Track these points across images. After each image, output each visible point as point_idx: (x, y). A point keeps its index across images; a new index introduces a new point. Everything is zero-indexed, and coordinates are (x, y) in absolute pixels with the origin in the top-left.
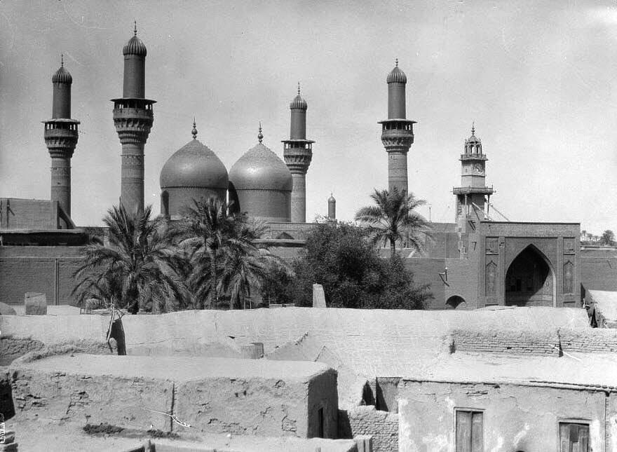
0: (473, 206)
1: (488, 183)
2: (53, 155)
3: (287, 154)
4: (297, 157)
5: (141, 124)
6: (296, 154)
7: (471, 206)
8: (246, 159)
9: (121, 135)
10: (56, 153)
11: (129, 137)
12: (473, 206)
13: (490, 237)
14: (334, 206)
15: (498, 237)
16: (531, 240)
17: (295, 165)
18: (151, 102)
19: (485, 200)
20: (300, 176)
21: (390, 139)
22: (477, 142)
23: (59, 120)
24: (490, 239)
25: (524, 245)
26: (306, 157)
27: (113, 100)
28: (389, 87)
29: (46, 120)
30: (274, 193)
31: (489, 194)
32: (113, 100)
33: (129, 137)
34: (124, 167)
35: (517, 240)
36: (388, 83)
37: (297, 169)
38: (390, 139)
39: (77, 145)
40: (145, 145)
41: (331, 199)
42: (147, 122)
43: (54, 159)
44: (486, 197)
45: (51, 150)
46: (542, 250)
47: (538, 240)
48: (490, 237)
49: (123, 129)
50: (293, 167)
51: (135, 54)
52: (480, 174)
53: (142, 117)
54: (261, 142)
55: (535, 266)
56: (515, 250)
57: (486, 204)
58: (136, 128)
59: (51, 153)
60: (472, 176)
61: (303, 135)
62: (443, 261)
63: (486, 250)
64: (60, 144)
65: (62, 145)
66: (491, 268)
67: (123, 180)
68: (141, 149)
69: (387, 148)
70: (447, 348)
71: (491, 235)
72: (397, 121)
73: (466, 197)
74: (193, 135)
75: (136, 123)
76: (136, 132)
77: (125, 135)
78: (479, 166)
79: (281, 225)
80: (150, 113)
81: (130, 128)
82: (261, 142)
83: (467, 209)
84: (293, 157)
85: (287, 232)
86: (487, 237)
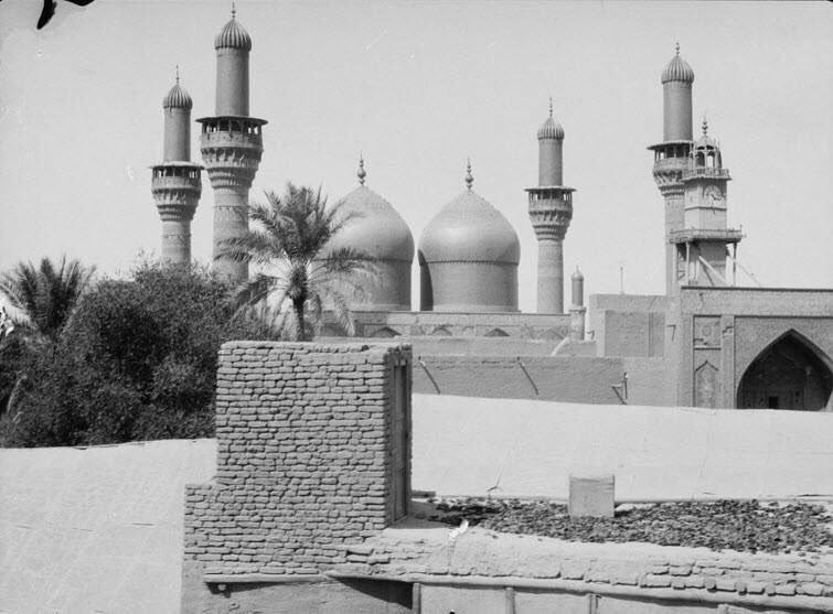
0: (701, 263)
1: (731, 222)
2: (165, 216)
3: (533, 209)
4: (547, 213)
5: (238, 156)
6: (547, 208)
7: (698, 263)
8: (448, 213)
9: (538, 230)
10: (167, 213)
11: (222, 178)
12: (701, 263)
13: (700, 316)
14: (581, 286)
15: (719, 316)
16: (792, 321)
17: (544, 226)
18: (260, 123)
19: (727, 253)
20: (553, 243)
21: (665, 174)
22: (709, 147)
23: (170, 164)
24: (702, 320)
25: (779, 331)
26: (561, 214)
27: (527, 190)
28: (665, 89)
29: (157, 164)
30: (483, 266)
31: (735, 241)
32: (527, 190)
33: (222, 178)
34: (540, 267)
35: (761, 321)
36: (664, 83)
37: (547, 233)
38: (665, 174)
39: (200, 202)
40: (250, 190)
41: (576, 276)
42: (254, 154)
43: (167, 223)
44: (730, 247)
45: (162, 210)
46: (815, 341)
47: (806, 323)
48: (700, 316)
49: (539, 224)
50: (221, 174)
51: (231, 47)
52: (717, 204)
53: (240, 145)
54: (470, 187)
55: (808, 373)
56: (757, 341)
57: (729, 261)
58: (230, 163)
59: (162, 213)
60: (700, 208)
61: (559, 178)
62: (619, 363)
63: (694, 340)
64: (171, 198)
65: (175, 201)
66: (706, 374)
67: (540, 280)
68: (560, 246)
69: (662, 189)
70: (495, 540)
71: (704, 313)
72: (675, 144)
73: (688, 246)
74: (359, 179)
75: (231, 154)
76: (231, 170)
77: (542, 230)
78: (715, 191)
79: (492, 317)
80: (257, 140)
81: (222, 163)
82: (470, 187)
83: (694, 270)
84: (540, 213)
85: (502, 329)
86: (695, 316)
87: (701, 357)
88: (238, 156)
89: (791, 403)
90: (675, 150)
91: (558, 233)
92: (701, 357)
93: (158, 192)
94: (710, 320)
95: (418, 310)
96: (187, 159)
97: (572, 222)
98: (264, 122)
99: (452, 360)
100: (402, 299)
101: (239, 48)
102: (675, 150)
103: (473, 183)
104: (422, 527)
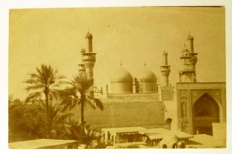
20: (166, 77)
25: (203, 93)
61: (167, 63)
87: (183, 100)
88: (86, 61)
89: (11, 113)
90: (88, 55)
91: (167, 75)
92: (183, 100)
93: (162, 72)
94: (184, 91)
95: (135, 93)
96: (167, 65)
97: (170, 73)
98: (96, 54)
99: (120, 103)
100: (131, 90)
101: (90, 38)
102: (88, 55)
103: (122, 65)
104: (25, 141)
